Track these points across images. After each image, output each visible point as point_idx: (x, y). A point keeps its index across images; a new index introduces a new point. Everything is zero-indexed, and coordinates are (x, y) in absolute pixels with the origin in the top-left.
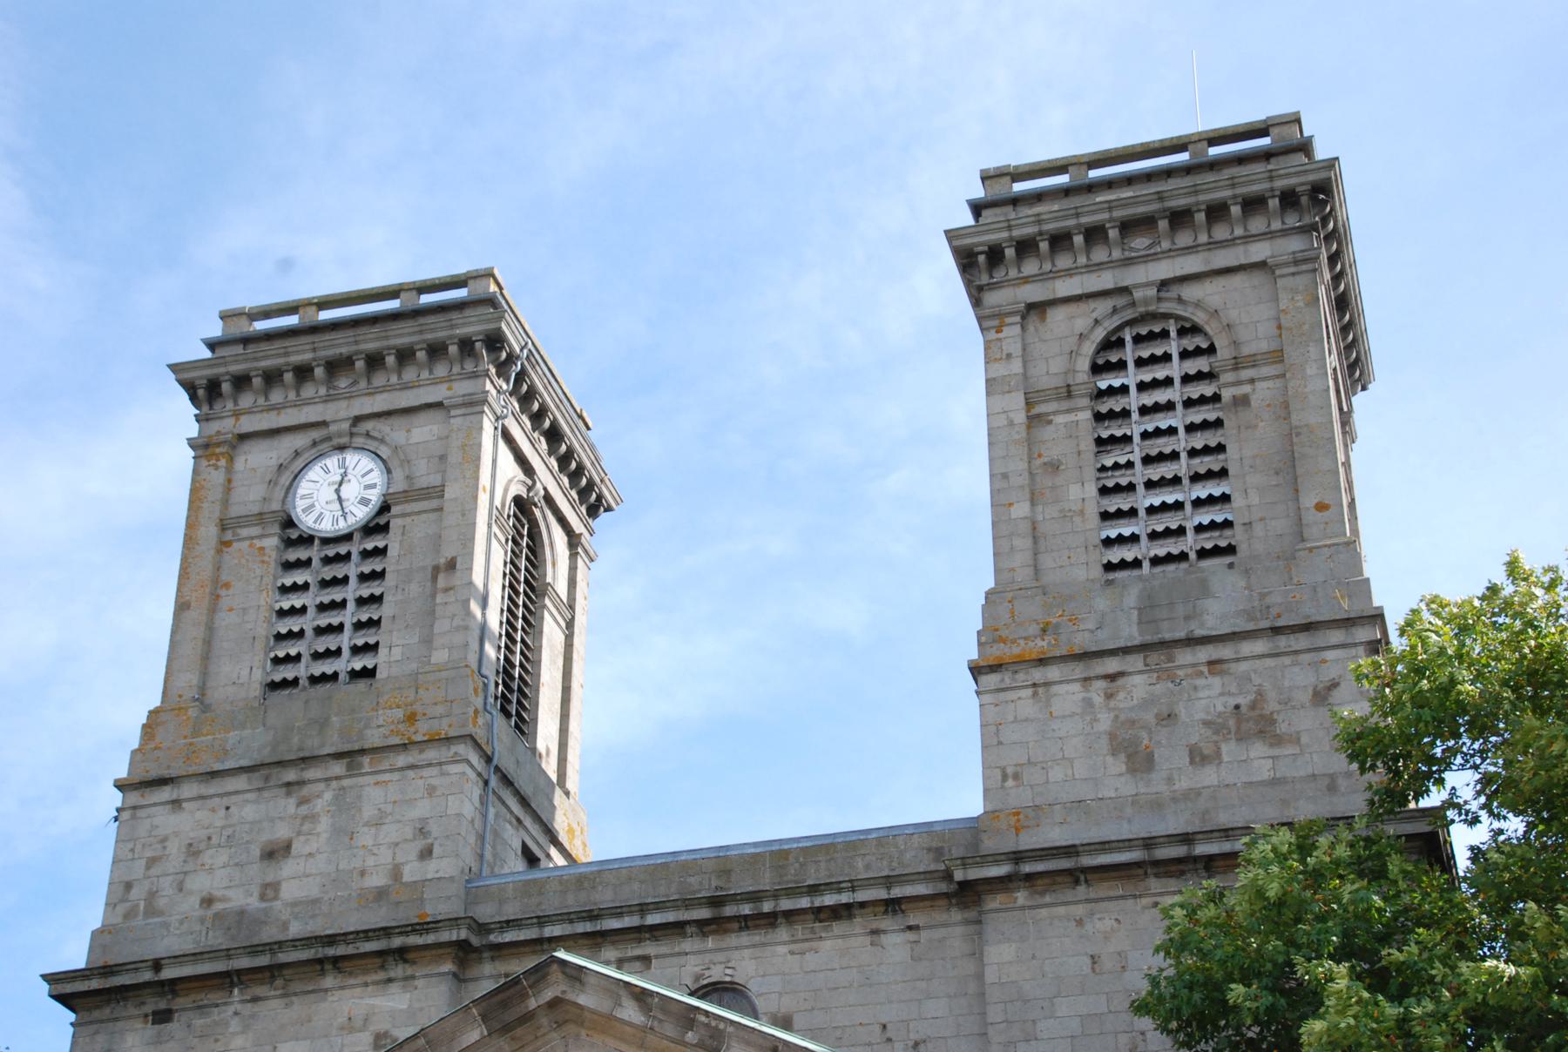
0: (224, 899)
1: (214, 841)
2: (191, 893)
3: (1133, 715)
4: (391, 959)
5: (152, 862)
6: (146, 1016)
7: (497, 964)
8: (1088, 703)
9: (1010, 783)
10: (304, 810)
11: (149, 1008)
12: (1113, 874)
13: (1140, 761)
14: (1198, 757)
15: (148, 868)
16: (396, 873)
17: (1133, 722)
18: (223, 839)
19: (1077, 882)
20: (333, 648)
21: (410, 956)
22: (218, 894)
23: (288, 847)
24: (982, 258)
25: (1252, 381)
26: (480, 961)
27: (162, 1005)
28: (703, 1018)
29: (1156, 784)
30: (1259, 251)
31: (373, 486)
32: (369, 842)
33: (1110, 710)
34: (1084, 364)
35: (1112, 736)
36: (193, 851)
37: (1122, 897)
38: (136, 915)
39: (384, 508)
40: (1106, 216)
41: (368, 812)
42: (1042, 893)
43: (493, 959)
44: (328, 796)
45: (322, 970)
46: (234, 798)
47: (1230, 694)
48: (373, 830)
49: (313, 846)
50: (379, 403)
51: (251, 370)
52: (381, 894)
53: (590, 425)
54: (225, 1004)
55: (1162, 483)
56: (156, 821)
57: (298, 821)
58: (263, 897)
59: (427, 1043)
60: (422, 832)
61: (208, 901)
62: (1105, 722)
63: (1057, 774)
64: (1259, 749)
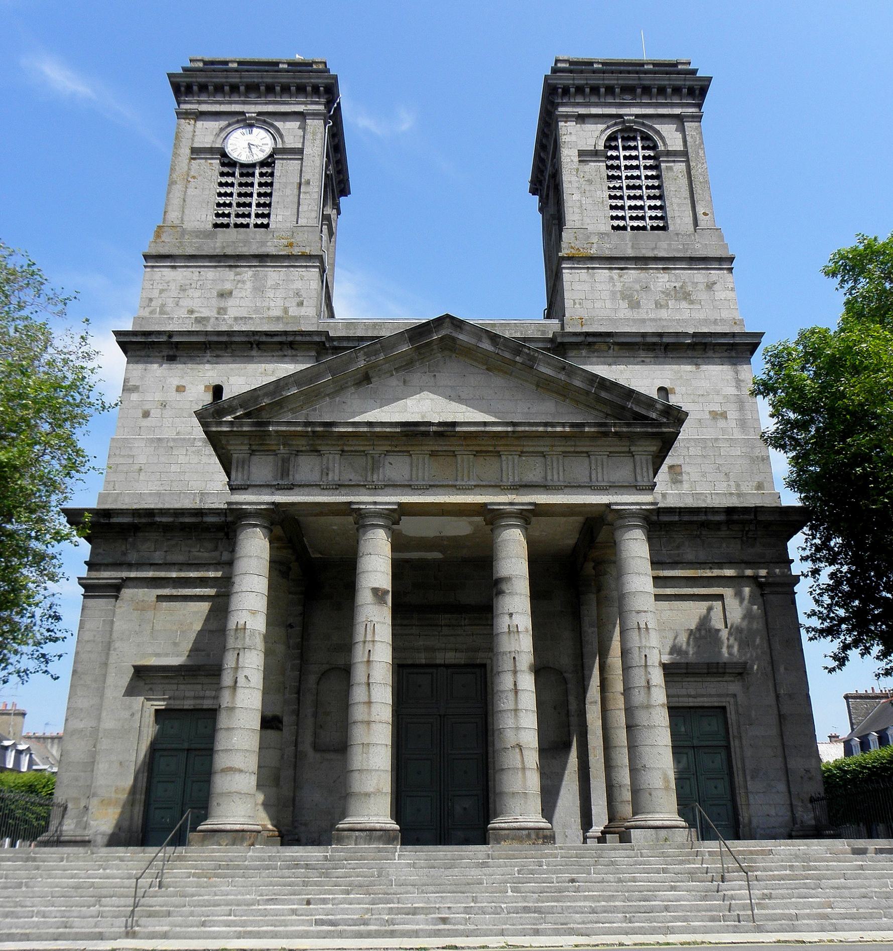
2: (182, 307)
4: (285, 346)
5: (162, 291)
6: (163, 357)
8: (611, 278)
9: (577, 306)
11: (165, 354)
12: (626, 347)
13: (635, 305)
14: (658, 305)
15: (160, 293)
16: (286, 310)
21: (295, 346)
22: (197, 309)
23: (230, 293)
24: (560, 90)
27: (171, 353)
28: (527, 351)
29: (641, 314)
32: (272, 296)
35: (622, 292)
36: (183, 289)
37: (629, 357)
40: (616, 82)
41: (270, 283)
45: (251, 347)
47: (671, 282)
48: (273, 291)
49: (243, 294)
51: (209, 82)
52: (278, 319)
53: (166, 274)
54: (203, 356)
55: (635, 198)
56: (164, 273)
57: (235, 283)
58: (219, 313)
59: (381, 347)
60: (298, 294)
61: (191, 312)
62: (619, 287)
63: (598, 305)
64: (684, 304)
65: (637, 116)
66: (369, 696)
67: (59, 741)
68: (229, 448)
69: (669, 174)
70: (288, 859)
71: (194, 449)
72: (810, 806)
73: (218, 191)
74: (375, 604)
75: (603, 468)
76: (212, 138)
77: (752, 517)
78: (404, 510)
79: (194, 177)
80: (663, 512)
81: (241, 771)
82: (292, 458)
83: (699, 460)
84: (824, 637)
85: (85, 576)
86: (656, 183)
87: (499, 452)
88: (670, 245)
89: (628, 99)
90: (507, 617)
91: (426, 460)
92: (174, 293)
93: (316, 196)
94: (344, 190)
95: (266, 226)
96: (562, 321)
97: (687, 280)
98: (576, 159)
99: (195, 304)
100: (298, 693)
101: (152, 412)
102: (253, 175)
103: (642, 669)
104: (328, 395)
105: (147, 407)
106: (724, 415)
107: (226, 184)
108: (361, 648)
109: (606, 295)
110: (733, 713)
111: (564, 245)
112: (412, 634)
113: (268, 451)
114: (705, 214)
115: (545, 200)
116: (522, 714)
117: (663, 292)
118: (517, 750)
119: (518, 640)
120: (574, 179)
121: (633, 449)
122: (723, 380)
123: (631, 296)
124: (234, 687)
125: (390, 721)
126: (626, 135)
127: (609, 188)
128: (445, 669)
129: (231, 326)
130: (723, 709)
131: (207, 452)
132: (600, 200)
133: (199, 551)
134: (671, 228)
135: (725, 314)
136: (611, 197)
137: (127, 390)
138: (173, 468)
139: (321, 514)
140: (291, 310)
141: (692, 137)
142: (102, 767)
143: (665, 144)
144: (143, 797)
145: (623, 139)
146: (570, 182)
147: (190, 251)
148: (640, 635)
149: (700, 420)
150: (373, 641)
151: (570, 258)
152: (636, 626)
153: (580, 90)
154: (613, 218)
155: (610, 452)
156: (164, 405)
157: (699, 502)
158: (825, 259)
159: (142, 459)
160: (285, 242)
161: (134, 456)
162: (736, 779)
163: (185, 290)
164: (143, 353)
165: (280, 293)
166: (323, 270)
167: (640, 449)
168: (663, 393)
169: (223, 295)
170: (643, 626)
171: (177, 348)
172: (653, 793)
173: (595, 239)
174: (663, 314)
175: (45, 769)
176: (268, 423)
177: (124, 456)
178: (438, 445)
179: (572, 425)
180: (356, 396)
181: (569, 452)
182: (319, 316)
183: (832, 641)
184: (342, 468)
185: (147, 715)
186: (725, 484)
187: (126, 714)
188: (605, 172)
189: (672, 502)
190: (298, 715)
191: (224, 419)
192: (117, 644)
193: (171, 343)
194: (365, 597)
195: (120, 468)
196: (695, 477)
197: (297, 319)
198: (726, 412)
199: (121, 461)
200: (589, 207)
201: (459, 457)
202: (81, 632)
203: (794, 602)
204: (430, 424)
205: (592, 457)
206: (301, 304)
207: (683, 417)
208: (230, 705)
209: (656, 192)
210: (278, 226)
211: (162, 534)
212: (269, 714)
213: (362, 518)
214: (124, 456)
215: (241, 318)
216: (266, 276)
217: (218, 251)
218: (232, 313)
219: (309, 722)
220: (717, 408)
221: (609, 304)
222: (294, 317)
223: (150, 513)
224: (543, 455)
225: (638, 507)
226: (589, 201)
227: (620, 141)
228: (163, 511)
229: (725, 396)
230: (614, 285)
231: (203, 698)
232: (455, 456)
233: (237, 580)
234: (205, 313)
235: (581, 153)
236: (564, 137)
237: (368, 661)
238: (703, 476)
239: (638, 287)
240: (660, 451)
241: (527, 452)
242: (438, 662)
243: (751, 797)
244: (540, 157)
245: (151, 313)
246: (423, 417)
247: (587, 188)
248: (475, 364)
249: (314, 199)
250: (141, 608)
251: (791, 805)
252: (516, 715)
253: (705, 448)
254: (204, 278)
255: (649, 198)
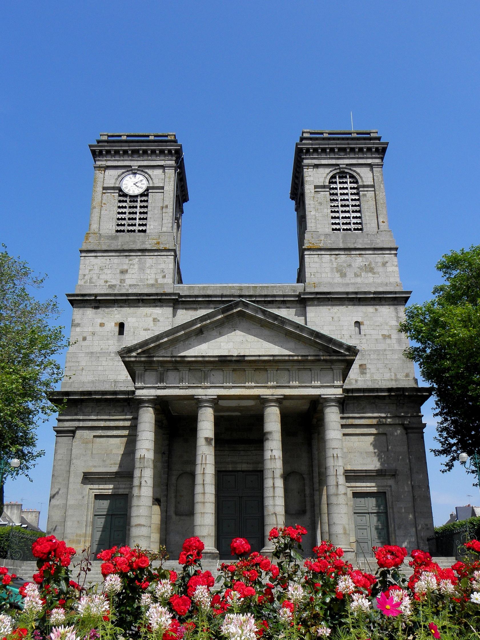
0: (111, 282)
1: (107, 267)
2: (101, 279)
3: (341, 264)
5: (90, 270)
7: (183, 305)
8: (331, 260)
9: (312, 276)
10: (131, 262)
13: (343, 275)
14: (356, 275)
15: (89, 272)
16: (156, 280)
17: (342, 266)
18: (109, 267)
19: (329, 300)
20: (134, 224)
22: (109, 280)
25: (367, 191)
26: (179, 304)
27: (96, 305)
28: (280, 318)
29: (347, 280)
30: (369, 161)
31: (144, 184)
32: (149, 272)
33: (336, 262)
34: (327, 181)
35: (336, 268)
36: (101, 269)
38: (87, 283)
39: (147, 190)
41: (148, 265)
42: (321, 302)
43: (182, 304)
44: (137, 260)
46: (111, 257)
47: (364, 262)
48: (150, 269)
50: (145, 163)
52: (153, 285)
55: (345, 212)
57: (129, 265)
58: (121, 282)
60: (163, 271)
61: (106, 282)
62: (335, 265)
63: (324, 275)
64: (370, 275)
65: (347, 165)
66: (204, 490)
67: (11, 507)
68: (134, 368)
69: (364, 198)
70: (168, 566)
71: (110, 357)
72: (427, 543)
73: (118, 211)
74: (206, 445)
75: (317, 377)
76: (113, 181)
77: (402, 393)
78: (220, 397)
79: (105, 204)
80: (355, 391)
81: (144, 526)
82: (165, 373)
83: (375, 362)
84: (443, 454)
85: (57, 426)
86: (357, 203)
87: (266, 369)
88: (363, 240)
89: (342, 155)
90: (270, 451)
91: (231, 373)
92: (97, 271)
93: (171, 214)
94: (186, 199)
95: (144, 231)
96: (305, 284)
97: (372, 261)
98: (313, 191)
99: (108, 277)
100: (167, 486)
101: (88, 337)
102: (137, 201)
103: (335, 477)
104: (182, 341)
105: (85, 335)
106: (389, 337)
107: (123, 207)
108: (200, 467)
109: (328, 270)
110: (389, 495)
111: (306, 241)
112: (225, 455)
113: (153, 369)
114: (383, 222)
115: (298, 205)
116: (277, 499)
117: (359, 268)
118: (274, 515)
119: (275, 463)
120: (312, 202)
121: (332, 367)
122: (390, 317)
123: (342, 270)
124: (140, 486)
125: (214, 502)
126: (341, 175)
127: (331, 206)
128: (241, 473)
129: (128, 290)
130: (385, 493)
131: (117, 360)
132: (326, 214)
133: (115, 412)
134: (365, 230)
135: (392, 280)
136: (332, 212)
137: (74, 326)
138: (100, 368)
139: (179, 400)
140: (159, 280)
141: (377, 177)
142: (69, 524)
143: (363, 181)
144: (90, 539)
145: (339, 177)
146: (310, 204)
147: (104, 248)
148: (334, 460)
149: (377, 339)
150: (206, 464)
151: (309, 249)
152: (332, 455)
153: (315, 150)
154: (333, 224)
155: (321, 369)
156: (94, 334)
157: (375, 384)
158: (440, 258)
159: (83, 363)
160: (155, 241)
161: (79, 362)
162: (390, 529)
163: (102, 270)
164: (82, 305)
165: (154, 271)
166: (175, 256)
167: (336, 367)
168: (358, 325)
169: (123, 272)
170: (335, 455)
171: (99, 302)
172: (338, 536)
173: (322, 238)
174: (359, 280)
175: (6, 524)
176: (154, 357)
177: (74, 362)
178: (237, 366)
179: (302, 356)
180: (196, 341)
181: (301, 369)
182: (174, 282)
183: (447, 456)
184: (190, 377)
185: (91, 497)
186: (389, 374)
187: (80, 497)
188: (329, 197)
189: (361, 385)
190: (167, 497)
191: (132, 355)
192: (74, 461)
193: (97, 300)
194: (201, 442)
195: (72, 368)
196: (373, 370)
197: (162, 285)
198: (390, 335)
199: (72, 364)
200: (320, 218)
201: (247, 372)
202: (56, 455)
203: (423, 438)
204: (232, 356)
205: (313, 371)
206: (164, 277)
207: (357, 352)
208: (138, 495)
209: (357, 208)
210: (151, 231)
211: (95, 403)
212: (155, 498)
213: (200, 403)
214: (74, 362)
215: (133, 285)
216: (145, 261)
217: (119, 248)
218: (128, 282)
219: (173, 500)
220: (386, 333)
221: (329, 275)
222: (161, 284)
223: (89, 393)
224: (288, 370)
225: (334, 396)
226: (320, 214)
227: (337, 178)
228: (96, 392)
229: (391, 326)
230: (332, 264)
231: (119, 488)
232: (245, 371)
233: (139, 434)
234: (114, 282)
235: (316, 187)
236: (306, 178)
237: (204, 473)
238: (378, 370)
239: (345, 265)
240: (347, 366)
241: (280, 369)
242: (238, 469)
243: (397, 538)
244: (295, 182)
245: (85, 282)
246: (229, 351)
247: (319, 207)
248: (254, 323)
249: (170, 216)
250: (86, 442)
251: (418, 542)
252: (274, 499)
253: (379, 355)
254: (112, 262)
255: (353, 212)
